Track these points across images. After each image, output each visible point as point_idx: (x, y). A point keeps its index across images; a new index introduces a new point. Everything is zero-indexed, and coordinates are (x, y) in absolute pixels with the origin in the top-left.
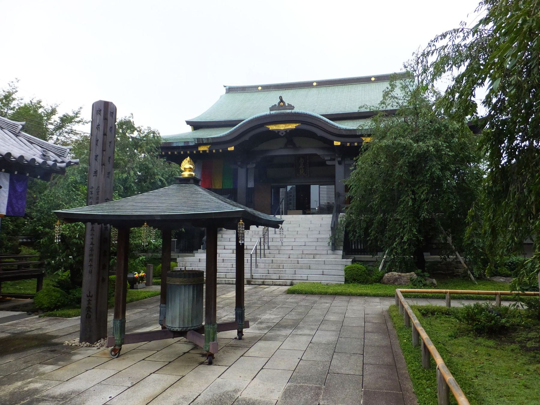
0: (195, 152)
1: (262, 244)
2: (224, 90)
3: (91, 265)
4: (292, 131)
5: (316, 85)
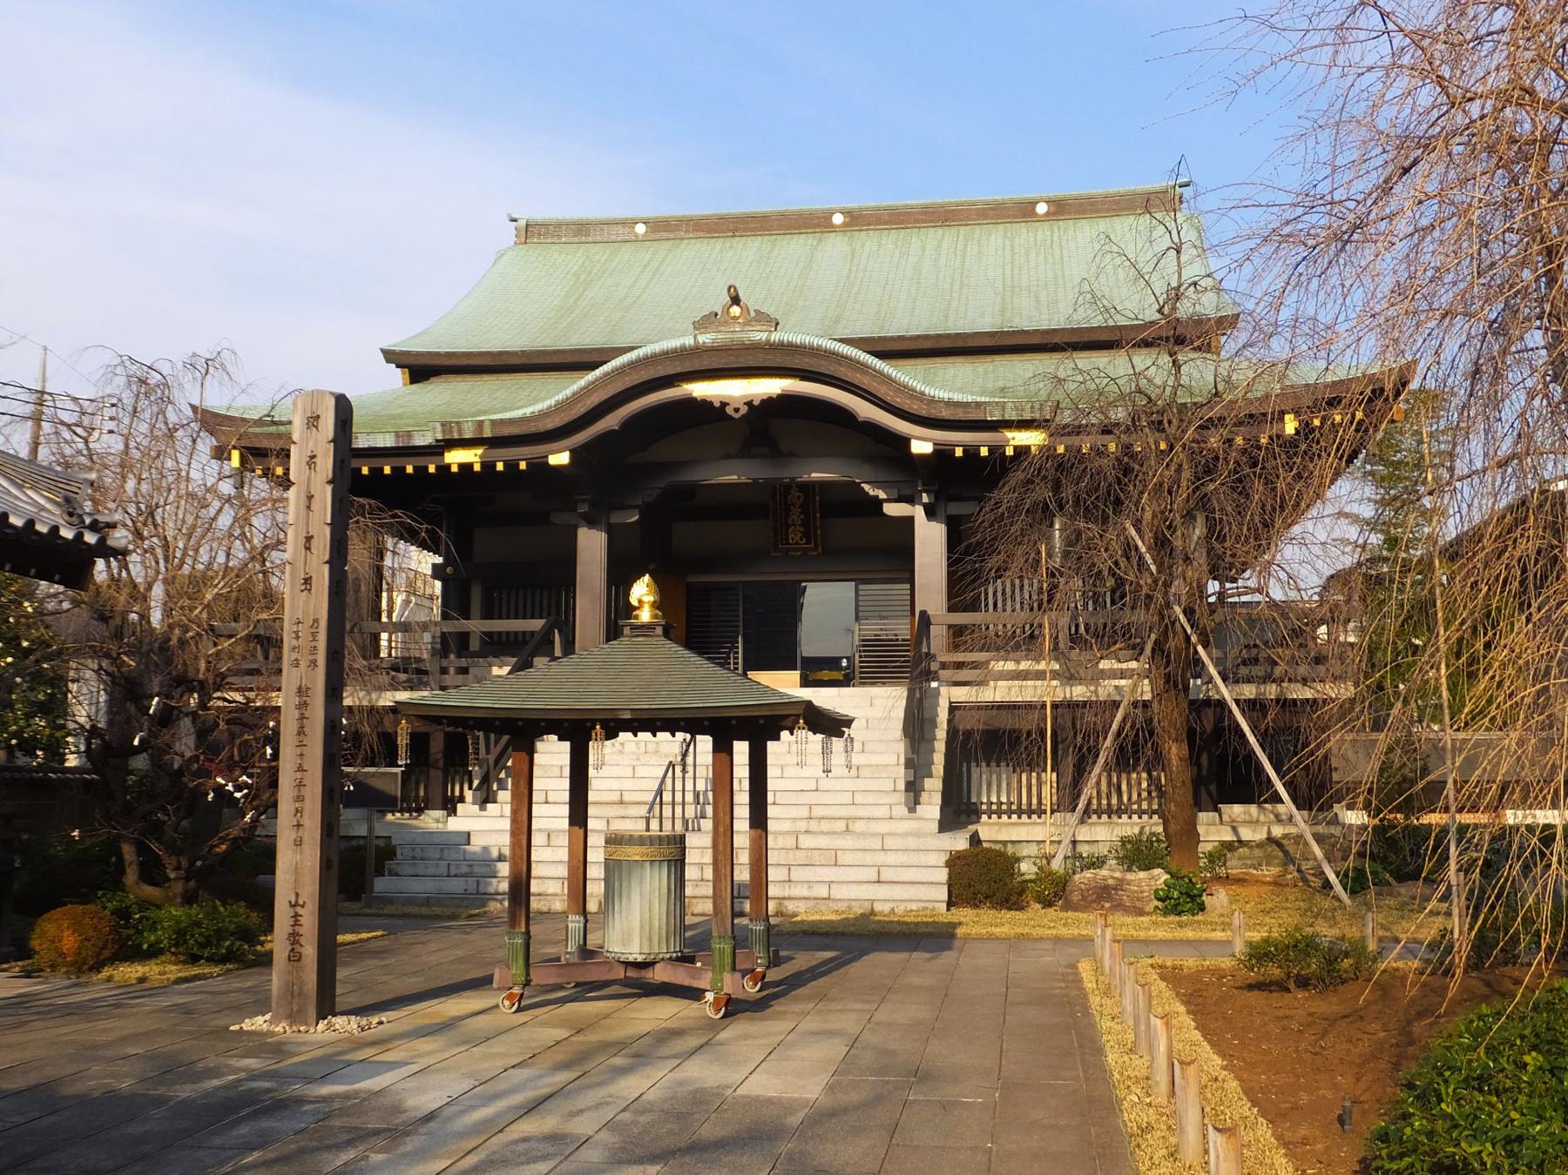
0: (432, 469)
2: (509, 233)
3: (299, 825)
5: (845, 224)
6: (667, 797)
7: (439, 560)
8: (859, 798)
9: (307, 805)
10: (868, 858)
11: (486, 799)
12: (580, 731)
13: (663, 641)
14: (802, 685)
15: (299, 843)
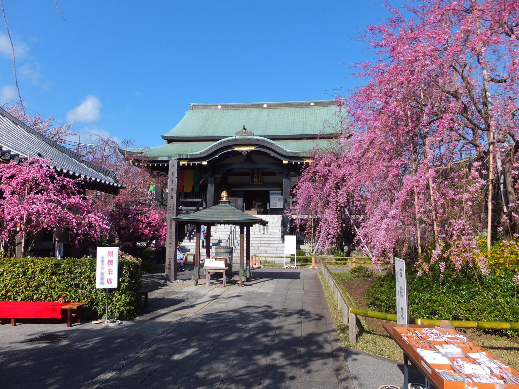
4: (252, 152)
6: (231, 238)
8: (271, 239)
9: (172, 240)
10: (274, 252)
11: (190, 238)
12: (210, 224)
13: (228, 205)
14: (258, 214)
15: (170, 247)
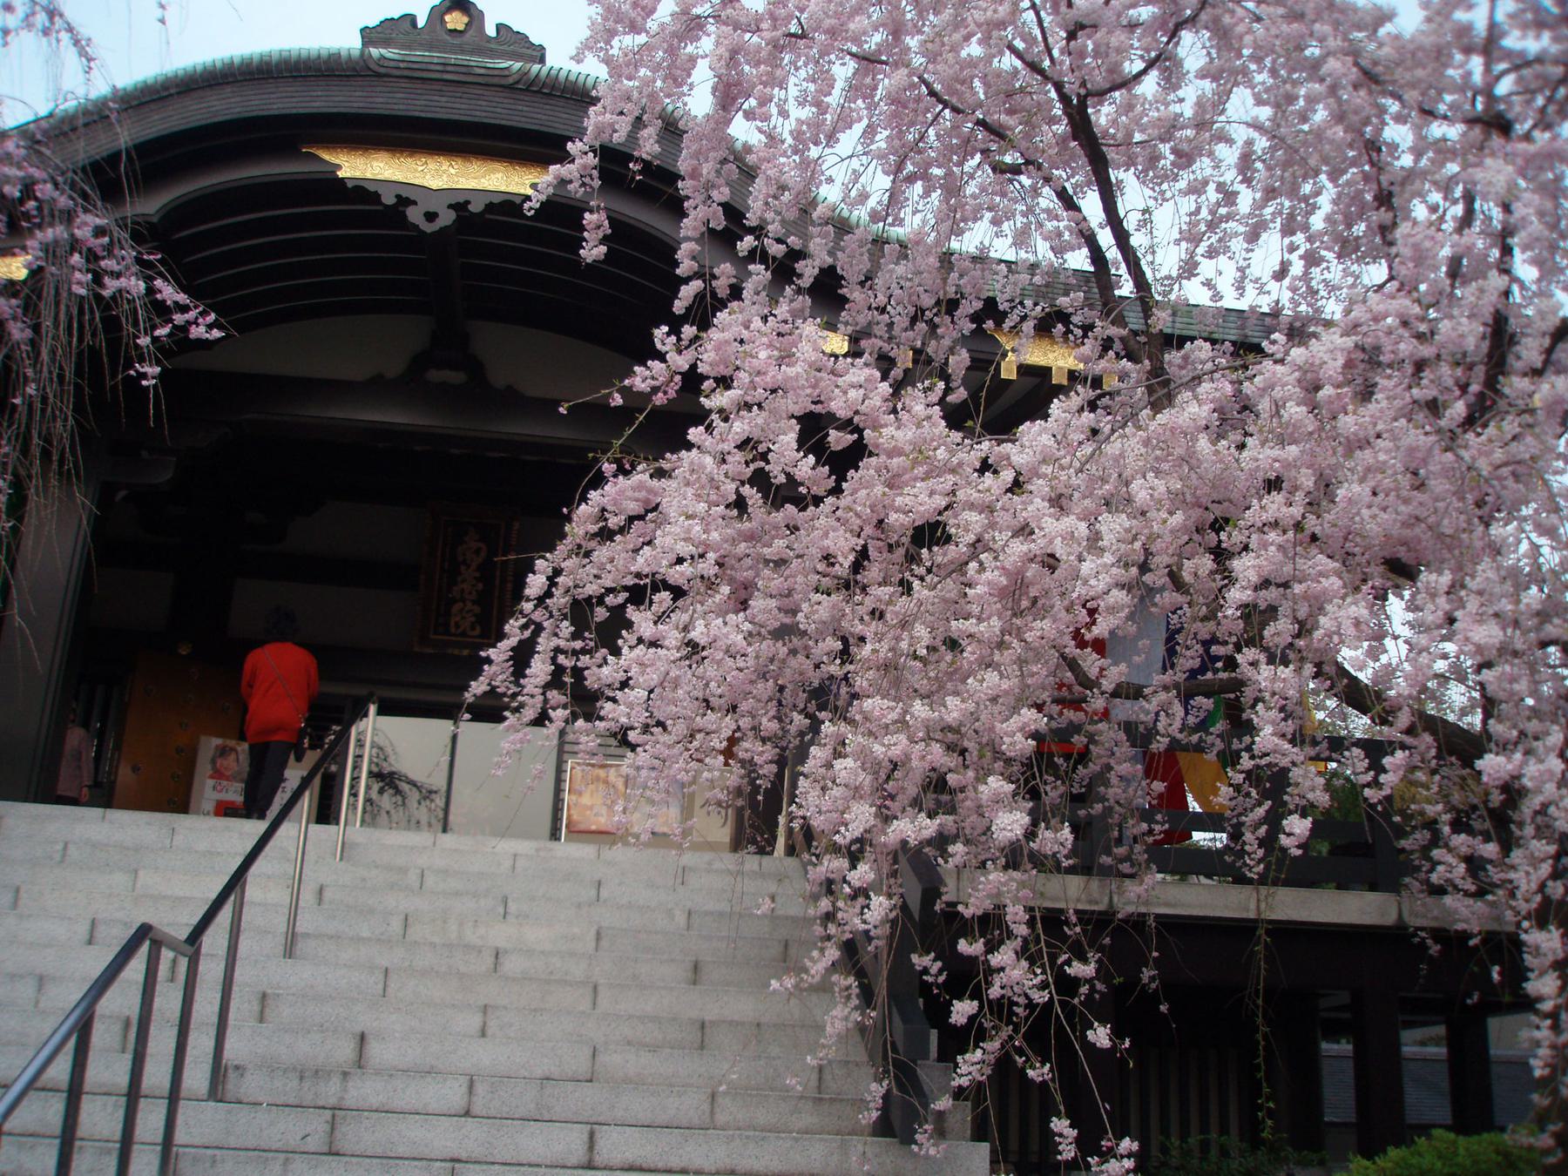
1: (162, 1042)
7: (421, 23)
